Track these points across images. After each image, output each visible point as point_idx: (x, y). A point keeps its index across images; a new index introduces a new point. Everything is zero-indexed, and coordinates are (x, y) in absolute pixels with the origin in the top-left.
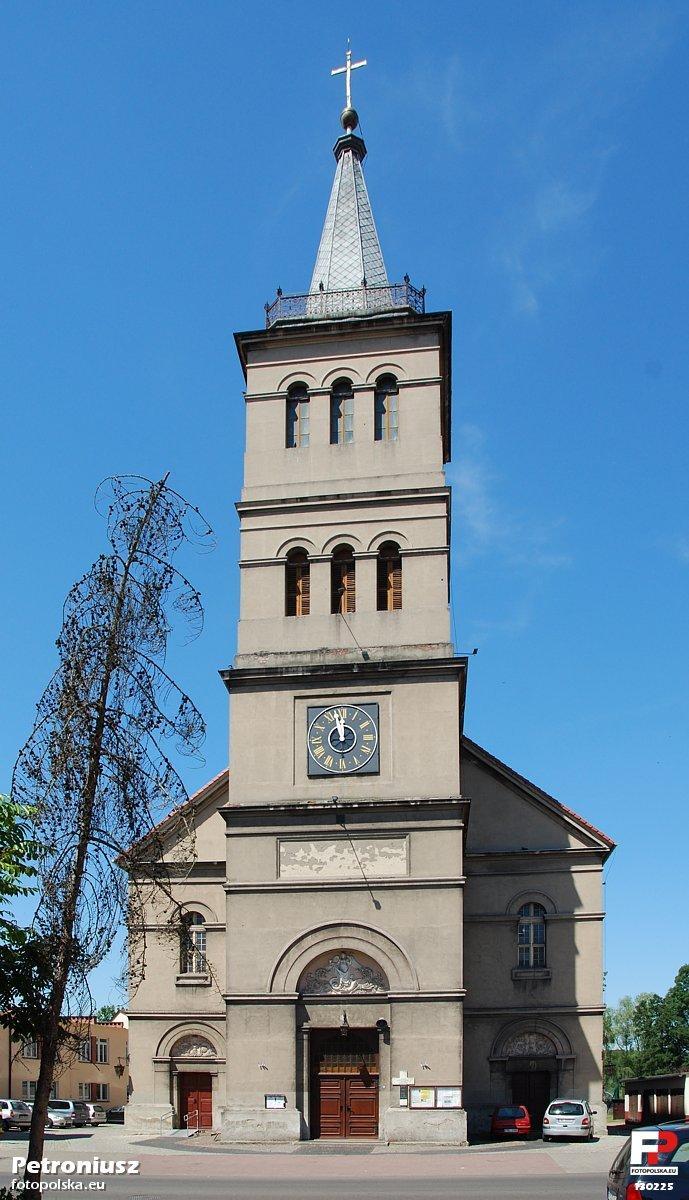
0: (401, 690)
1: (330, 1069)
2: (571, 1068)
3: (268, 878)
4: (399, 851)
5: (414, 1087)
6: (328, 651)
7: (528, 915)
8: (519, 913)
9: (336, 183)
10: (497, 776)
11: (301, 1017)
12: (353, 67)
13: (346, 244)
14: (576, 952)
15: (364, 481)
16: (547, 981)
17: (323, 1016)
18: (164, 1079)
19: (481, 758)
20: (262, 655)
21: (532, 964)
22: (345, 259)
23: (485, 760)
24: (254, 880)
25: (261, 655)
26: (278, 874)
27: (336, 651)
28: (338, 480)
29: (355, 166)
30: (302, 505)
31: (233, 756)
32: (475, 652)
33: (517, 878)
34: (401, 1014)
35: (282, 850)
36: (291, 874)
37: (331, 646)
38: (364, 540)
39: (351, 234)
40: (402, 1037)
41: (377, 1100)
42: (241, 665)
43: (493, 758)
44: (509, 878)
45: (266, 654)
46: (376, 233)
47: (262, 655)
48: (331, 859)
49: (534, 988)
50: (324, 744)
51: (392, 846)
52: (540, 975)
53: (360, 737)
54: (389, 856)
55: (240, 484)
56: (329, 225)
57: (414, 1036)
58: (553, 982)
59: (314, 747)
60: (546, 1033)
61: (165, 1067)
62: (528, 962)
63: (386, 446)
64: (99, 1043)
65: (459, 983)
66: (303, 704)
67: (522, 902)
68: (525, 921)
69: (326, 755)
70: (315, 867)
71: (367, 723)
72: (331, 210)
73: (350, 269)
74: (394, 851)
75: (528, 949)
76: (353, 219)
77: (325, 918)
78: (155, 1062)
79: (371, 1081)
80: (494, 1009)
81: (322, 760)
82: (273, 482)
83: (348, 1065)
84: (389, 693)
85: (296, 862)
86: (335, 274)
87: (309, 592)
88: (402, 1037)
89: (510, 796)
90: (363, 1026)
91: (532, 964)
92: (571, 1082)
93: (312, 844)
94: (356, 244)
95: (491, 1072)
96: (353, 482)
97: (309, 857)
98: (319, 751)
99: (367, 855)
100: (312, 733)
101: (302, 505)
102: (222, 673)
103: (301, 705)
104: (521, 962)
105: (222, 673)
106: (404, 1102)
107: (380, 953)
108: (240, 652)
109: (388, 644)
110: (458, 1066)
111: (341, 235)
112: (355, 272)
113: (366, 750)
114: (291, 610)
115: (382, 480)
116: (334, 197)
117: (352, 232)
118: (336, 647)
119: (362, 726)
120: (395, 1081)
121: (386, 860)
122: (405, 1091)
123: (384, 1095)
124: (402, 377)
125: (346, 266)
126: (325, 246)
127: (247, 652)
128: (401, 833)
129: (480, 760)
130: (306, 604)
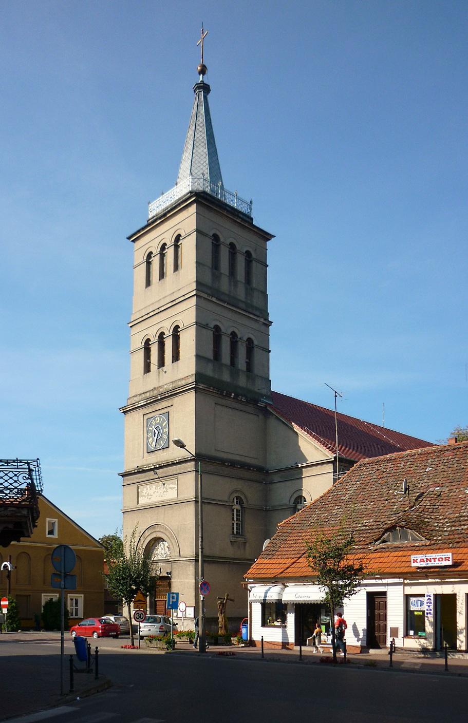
0: (176, 400)
26: (138, 503)
33: (294, 481)
35: (139, 490)
36: (143, 501)
44: (290, 482)
48: (154, 493)
51: (172, 484)
67: (296, 495)
93: (148, 486)
119: (164, 425)
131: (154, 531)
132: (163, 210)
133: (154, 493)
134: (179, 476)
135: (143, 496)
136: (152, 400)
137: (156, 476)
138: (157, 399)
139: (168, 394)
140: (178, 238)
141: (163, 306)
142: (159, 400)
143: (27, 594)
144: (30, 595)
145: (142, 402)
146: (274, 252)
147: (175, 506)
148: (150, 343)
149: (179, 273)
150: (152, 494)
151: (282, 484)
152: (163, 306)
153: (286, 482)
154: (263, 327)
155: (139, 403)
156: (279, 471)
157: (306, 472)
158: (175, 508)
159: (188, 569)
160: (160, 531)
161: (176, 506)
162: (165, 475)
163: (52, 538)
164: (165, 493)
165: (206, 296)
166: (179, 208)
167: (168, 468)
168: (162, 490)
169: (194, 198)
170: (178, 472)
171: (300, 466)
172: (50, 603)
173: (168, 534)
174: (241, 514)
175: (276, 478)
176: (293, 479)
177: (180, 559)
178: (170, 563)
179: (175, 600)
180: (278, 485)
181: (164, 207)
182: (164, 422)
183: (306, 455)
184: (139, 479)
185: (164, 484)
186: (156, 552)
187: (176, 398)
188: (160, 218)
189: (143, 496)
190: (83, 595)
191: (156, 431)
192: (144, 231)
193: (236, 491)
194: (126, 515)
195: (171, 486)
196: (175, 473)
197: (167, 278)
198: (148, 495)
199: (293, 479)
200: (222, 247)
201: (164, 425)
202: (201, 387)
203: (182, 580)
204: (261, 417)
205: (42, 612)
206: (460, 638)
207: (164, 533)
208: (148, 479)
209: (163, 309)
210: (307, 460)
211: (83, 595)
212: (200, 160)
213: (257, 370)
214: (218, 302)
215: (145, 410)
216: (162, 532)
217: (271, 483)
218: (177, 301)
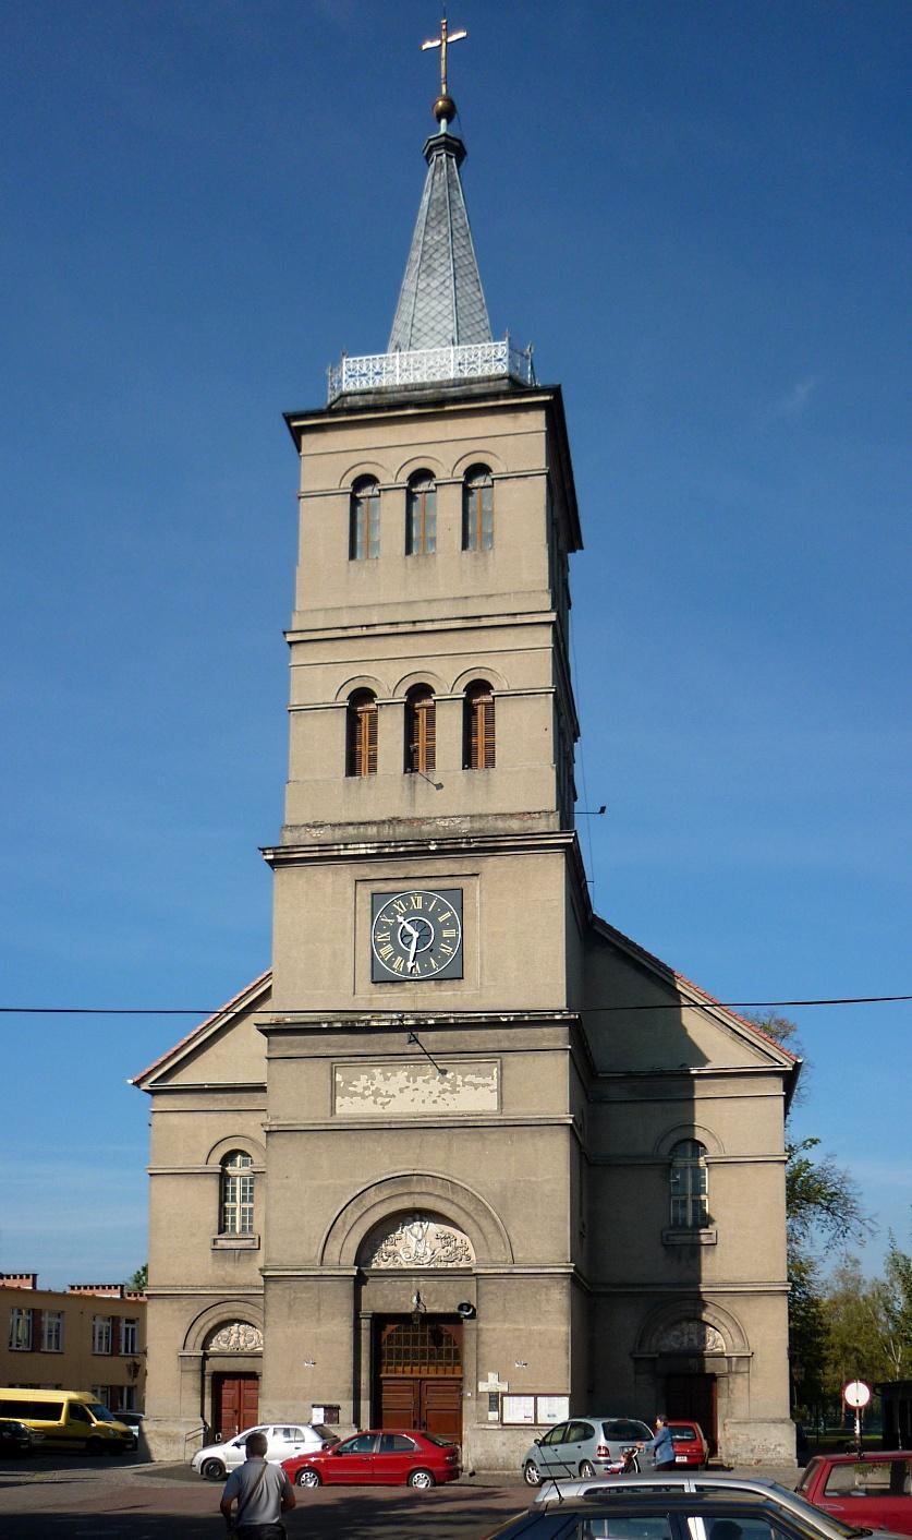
0: (491, 865)
1: (400, 1369)
2: (746, 1369)
3: (319, 1116)
4: (488, 1080)
5: (504, 1395)
6: (399, 821)
7: (685, 1157)
8: (670, 1154)
9: (426, 198)
12: (450, 40)
13: (434, 284)
15: (448, 603)
17: (390, 1298)
18: (192, 1381)
19: (618, 944)
20: (315, 826)
22: (434, 303)
23: (624, 948)
24: (302, 1121)
25: (314, 827)
26: (333, 1109)
27: (411, 821)
28: (415, 602)
29: (450, 174)
30: (369, 633)
31: (277, 957)
32: (603, 810)
33: (668, 1106)
34: (490, 1296)
35: (339, 1078)
36: (348, 1108)
37: (404, 815)
39: (442, 269)
40: (491, 1327)
41: (460, 1411)
42: (289, 838)
43: (634, 945)
44: (657, 1105)
45: (321, 826)
46: (476, 265)
47: (315, 826)
48: (401, 1090)
51: (479, 1074)
55: (289, 606)
56: (415, 255)
57: (507, 1326)
59: (379, 945)
61: (196, 1365)
62: (685, 1220)
63: (476, 558)
64: (123, 1325)
65: (565, 1255)
66: (365, 891)
67: (674, 1137)
69: (395, 956)
70: (380, 1100)
71: (448, 915)
72: (418, 234)
73: (439, 318)
74: (480, 1080)
76: (443, 249)
77: (393, 1168)
79: (458, 1385)
80: (639, 1285)
81: (390, 963)
82: (330, 604)
83: (398, 1364)
85: (356, 1094)
86: (418, 325)
87: (376, 744)
88: (491, 1327)
90: (442, 1311)
91: (690, 1223)
92: (746, 1391)
93: (377, 1071)
94: (447, 284)
95: (636, 1373)
96: (434, 604)
97: (373, 1088)
98: (387, 950)
99: (447, 1086)
100: (379, 927)
101: (369, 633)
103: (364, 892)
104: (676, 1220)
106: (493, 1416)
107: (463, 1213)
108: (287, 822)
109: (475, 812)
110: (564, 1366)
111: (429, 271)
112: (445, 322)
113: (446, 949)
114: (352, 769)
115: (469, 601)
116: (422, 217)
117: (444, 266)
118: (410, 815)
119: (441, 919)
120: (483, 1387)
121: (473, 1093)
122: (495, 1400)
123: (469, 1406)
125: (433, 314)
126: (409, 284)
127: (294, 823)
130: (373, 759)
131: (406, 1191)
132: (406, 388)
134: (509, 1058)
136: (402, 849)
138: (425, 848)
139: (466, 843)
141: (432, 621)
142: (430, 852)
145: (363, 846)
147: (493, 1133)
150: (397, 1093)
152: (432, 621)
155: (349, 847)
157: (701, 1089)
158: (493, 1137)
159: (544, 1297)
160: (431, 1194)
161: (496, 1135)
162: (450, 1048)
166: (491, 404)
167: (466, 1033)
168: (435, 1085)
169: (548, 398)
170: (505, 1045)
171: (693, 1072)
173: (463, 1203)
176: (668, 1100)
177: (515, 1271)
178: (474, 1278)
181: (496, 373)
183: (703, 1050)
184: (342, 1047)
185: (444, 1072)
186: (390, 1248)
187: (491, 859)
188: (419, 405)
191: (409, 928)
192: (349, 418)
194: (277, 1140)
196: (491, 1046)
199: (668, 1100)
203: (522, 1327)
206: (785, 1426)
208: (379, 1051)
209: (428, 627)
210: (705, 1061)
212: (424, 320)
215: (365, 871)
218: (485, 622)
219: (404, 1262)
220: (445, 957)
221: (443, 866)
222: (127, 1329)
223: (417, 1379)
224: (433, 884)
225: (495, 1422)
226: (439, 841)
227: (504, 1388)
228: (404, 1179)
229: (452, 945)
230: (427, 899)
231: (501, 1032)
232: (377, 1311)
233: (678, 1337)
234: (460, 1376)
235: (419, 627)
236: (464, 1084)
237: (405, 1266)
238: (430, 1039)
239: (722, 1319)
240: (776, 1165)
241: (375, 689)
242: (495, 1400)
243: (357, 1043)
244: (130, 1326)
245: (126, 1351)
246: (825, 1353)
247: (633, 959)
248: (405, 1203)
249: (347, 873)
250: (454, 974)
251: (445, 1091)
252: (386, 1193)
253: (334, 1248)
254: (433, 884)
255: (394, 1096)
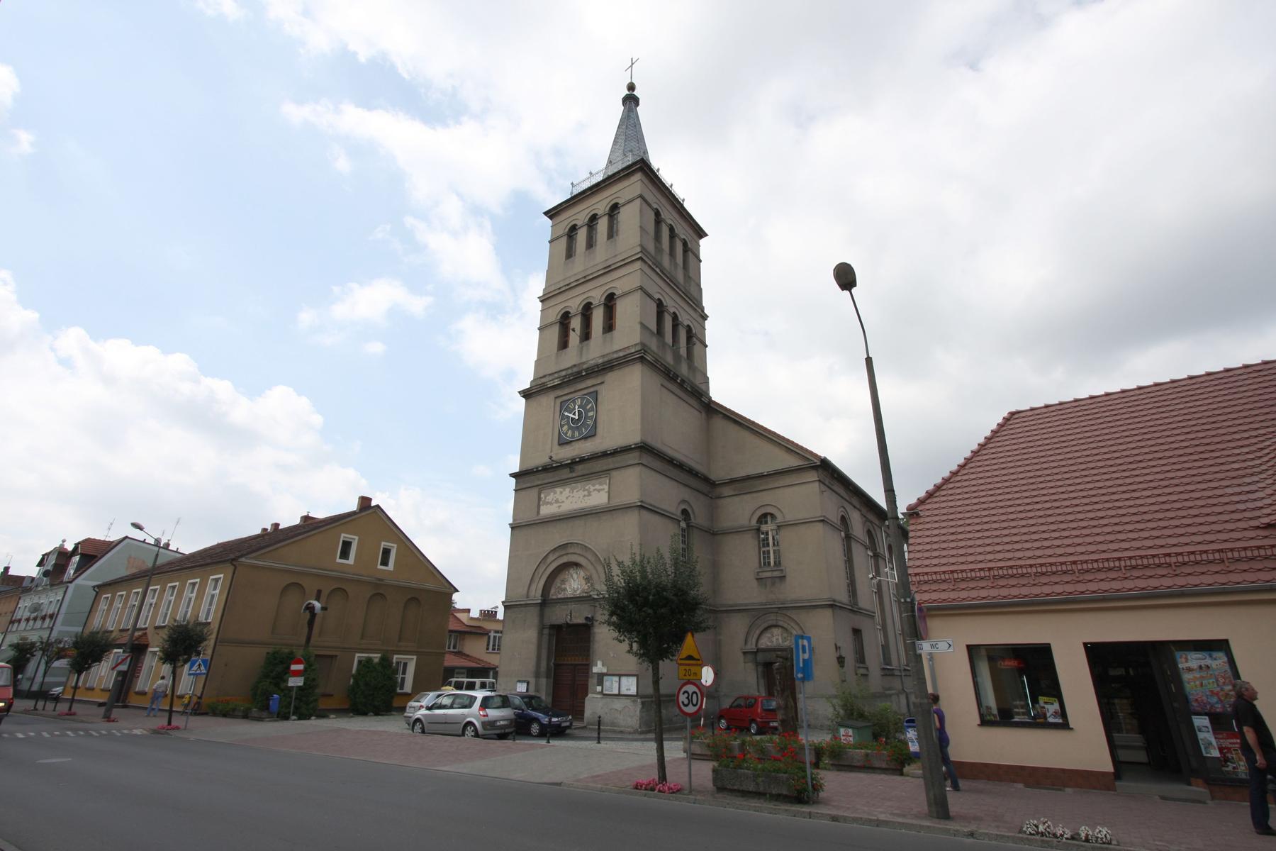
0: (610, 377)
10: (735, 422)
11: (542, 616)
14: (89, 539)
16: (783, 578)
21: (772, 563)
33: (755, 495)
35: (542, 496)
36: (546, 511)
38: (597, 296)
44: (748, 496)
48: (567, 498)
49: (773, 584)
50: (568, 424)
51: (600, 484)
52: (776, 574)
53: (586, 415)
54: (599, 491)
58: (788, 578)
59: (562, 426)
60: (785, 625)
62: (769, 563)
67: (759, 513)
68: (764, 528)
69: (568, 430)
74: (601, 487)
75: (769, 552)
78: (745, 653)
84: (603, 383)
89: (746, 435)
91: (772, 563)
102: (519, 392)
105: (519, 392)
106: (599, 689)
119: (588, 408)
124: (621, 201)
128: (607, 472)
129: (724, 414)
131: (564, 552)
133: (567, 498)
135: (548, 503)
137: (574, 475)
140: (615, 207)
142: (583, 376)
143: (334, 653)
144: (336, 656)
146: (705, 247)
148: (570, 315)
149: (615, 240)
150: (564, 499)
151: (736, 499)
153: (742, 496)
154: (700, 319)
156: (732, 481)
163: (385, 570)
164: (586, 498)
165: (651, 263)
172: (366, 664)
174: (686, 534)
175: (726, 491)
179: (806, 656)
180: (728, 500)
182: (588, 405)
189: (548, 503)
190: (415, 657)
193: (684, 501)
195: (597, 487)
197: (598, 247)
198: (557, 501)
200: (664, 225)
201: (588, 408)
202: (649, 359)
204: (704, 414)
205: (1172, 685)
207: (582, 556)
211: (415, 657)
213: (697, 363)
214: (661, 274)
215: (559, 393)
216: (579, 554)
217: (719, 497)
218: (613, 267)
219: (569, 593)
220: (589, 425)
221: (590, 382)
222: (495, 637)
223: (572, 665)
224: (585, 392)
225: (599, 693)
226: (586, 370)
227: (604, 670)
228: (564, 546)
229: (592, 419)
230: (582, 399)
231: (610, 460)
232: (552, 623)
233: (769, 638)
234: (587, 663)
235: (588, 278)
236: (594, 490)
237: (569, 596)
238: (580, 469)
239: (792, 624)
240: (817, 524)
241: (570, 311)
242: (601, 678)
243: (549, 477)
244: (498, 635)
245: (494, 649)
246: (79, 640)
247: (731, 418)
248: (564, 560)
249: (552, 395)
250: (592, 435)
251: (584, 496)
252: (557, 554)
253: (533, 587)
254: (585, 392)
255: (563, 502)
